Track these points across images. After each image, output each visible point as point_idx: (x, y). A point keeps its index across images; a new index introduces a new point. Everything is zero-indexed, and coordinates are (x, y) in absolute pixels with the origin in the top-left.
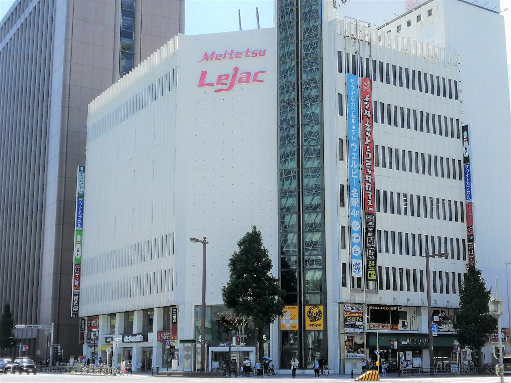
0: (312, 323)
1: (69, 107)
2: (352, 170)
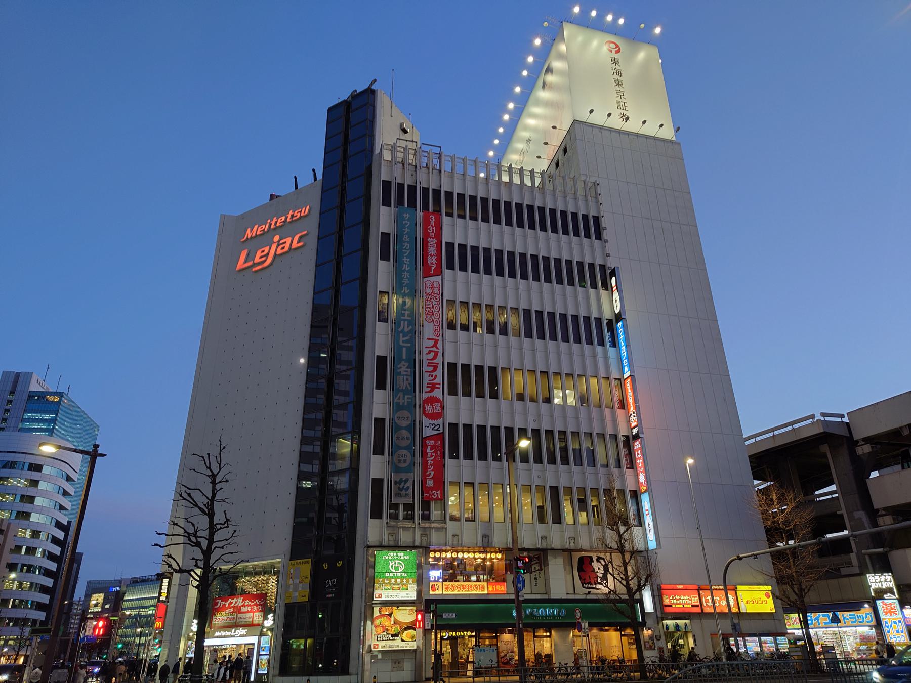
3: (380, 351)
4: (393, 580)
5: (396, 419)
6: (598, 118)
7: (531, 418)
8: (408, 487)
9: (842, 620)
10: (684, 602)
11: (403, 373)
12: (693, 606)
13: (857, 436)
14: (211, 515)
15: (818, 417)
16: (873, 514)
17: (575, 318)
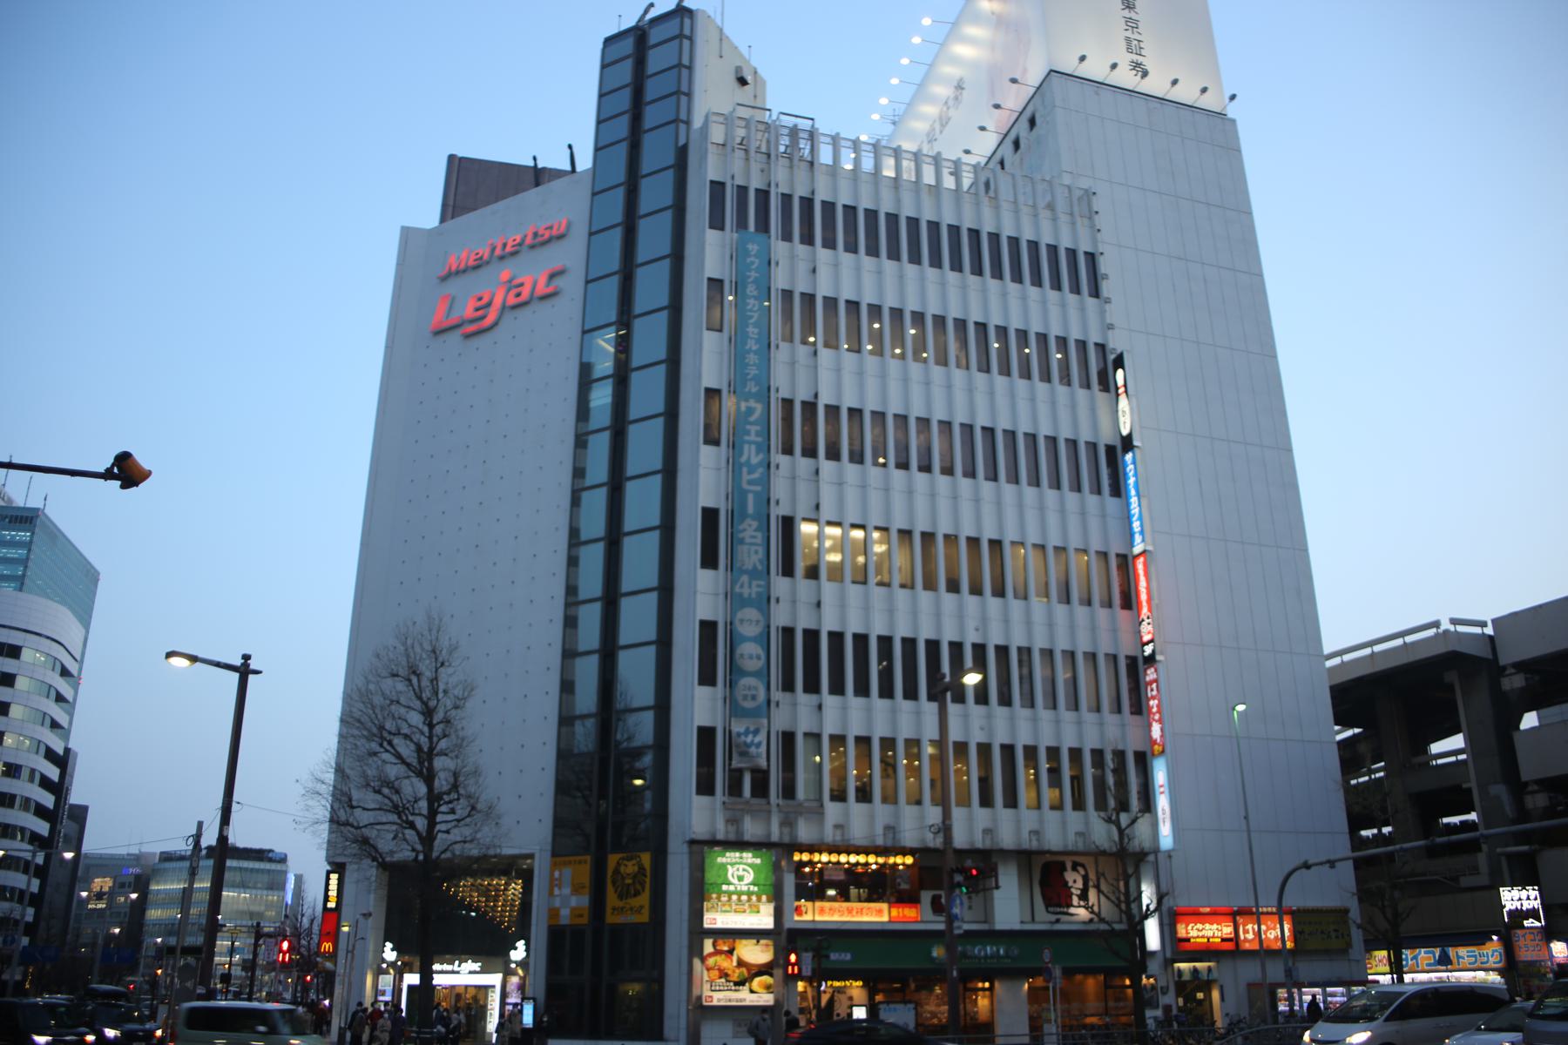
1: (1249, 831)
3: (707, 499)
4: (734, 897)
5: (737, 622)
6: (1095, 69)
7: (971, 624)
9: (1455, 960)
10: (1210, 934)
11: (748, 540)
12: (1223, 940)
13: (1504, 660)
14: (429, 778)
15: (1446, 625)
16: (1518, 788)
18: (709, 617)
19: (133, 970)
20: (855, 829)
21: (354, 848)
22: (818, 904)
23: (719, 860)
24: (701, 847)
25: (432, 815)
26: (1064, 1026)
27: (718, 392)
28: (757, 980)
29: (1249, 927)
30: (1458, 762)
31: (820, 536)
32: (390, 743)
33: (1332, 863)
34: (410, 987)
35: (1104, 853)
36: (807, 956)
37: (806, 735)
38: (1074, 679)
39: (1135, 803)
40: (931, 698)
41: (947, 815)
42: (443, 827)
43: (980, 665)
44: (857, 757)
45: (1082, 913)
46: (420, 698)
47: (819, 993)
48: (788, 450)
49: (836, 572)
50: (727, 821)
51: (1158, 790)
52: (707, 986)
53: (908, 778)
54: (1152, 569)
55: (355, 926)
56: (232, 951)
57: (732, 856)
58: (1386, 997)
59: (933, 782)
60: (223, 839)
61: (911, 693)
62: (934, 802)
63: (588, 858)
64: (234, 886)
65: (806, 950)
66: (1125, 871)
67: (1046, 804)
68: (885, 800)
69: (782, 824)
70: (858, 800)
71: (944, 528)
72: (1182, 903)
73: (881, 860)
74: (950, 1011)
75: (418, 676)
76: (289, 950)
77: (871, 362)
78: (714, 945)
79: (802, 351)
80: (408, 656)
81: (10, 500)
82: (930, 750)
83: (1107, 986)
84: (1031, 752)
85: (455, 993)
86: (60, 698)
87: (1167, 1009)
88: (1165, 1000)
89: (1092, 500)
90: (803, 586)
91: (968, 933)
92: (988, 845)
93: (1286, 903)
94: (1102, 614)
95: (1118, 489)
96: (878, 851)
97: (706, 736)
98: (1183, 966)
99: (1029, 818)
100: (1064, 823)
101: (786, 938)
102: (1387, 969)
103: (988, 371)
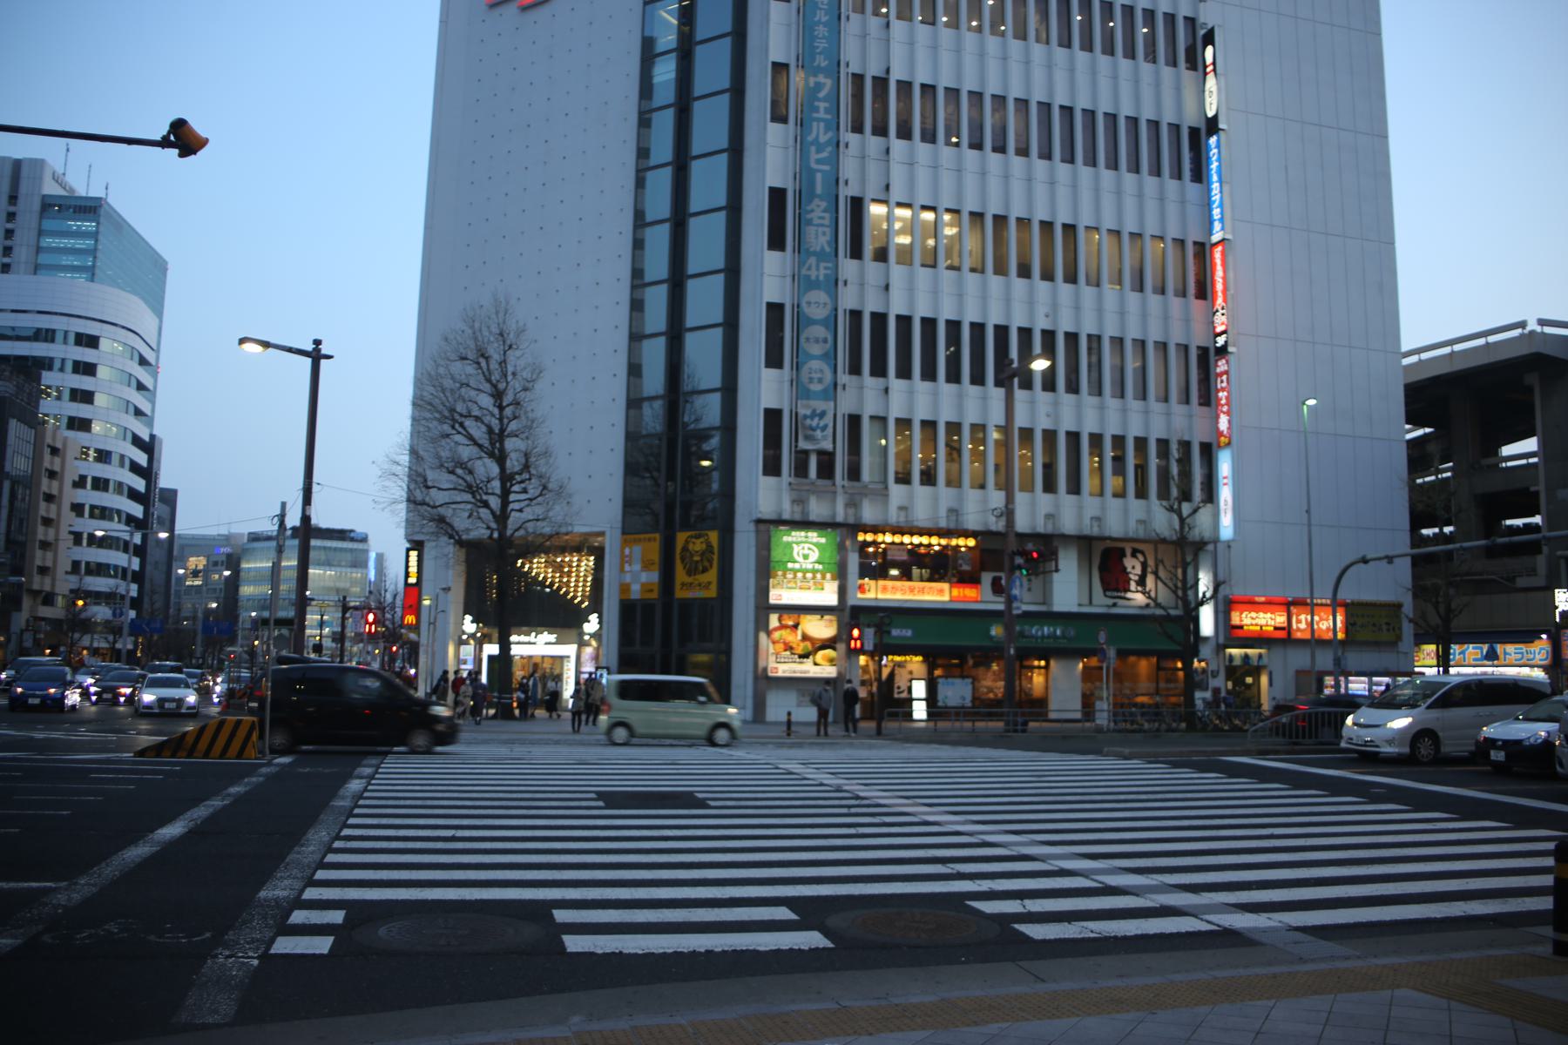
0: (690, 580)
1: (1309, 525)
2: (813, 149)
3: (774, 179)
4: (800, 575)
5: (804, 305)
7: (1041, 310)
8: (825, 427)
10: (1263, 622)
11: (816, 221)
12: (1276, 628)
14: (501, 459)
15: (1533, 326)
17: (1133, 121)
18: (776, 299)
19: (232, 641)
20: (918, 510)
21: (432, 527)
22: (881, 583)
23: (785, 539)
24: (767, 526)
25: (505, 494)
26: (1115, 705)
27: (786, 66)
28: (821, 653)
29: (1303, 617)
30: (1529, 464)
31: (889, 218)
32: (461, 425)
33: (1390, 559)
34: (491, 658)
35: (1164, 541)
36: (870, 632)
37: (872, 417)
38: (1144, 368)
39: (1197, 493)
40: (998, 383)
41: (1010, 499)
42: (516, 506)
43: (1049, 351)
44: (923, 441)
45: (1138, 598)
46: (489, 381)
47: (880, 666)
48: (858, 128)
49: (906, 255)
50: (793, 502)
51: (1222, 481)
52: (772, 658)
53: (972, 462)
54: (1230, 259)
55: (436, 599)
56: (322, 624)
57: (797, 535)
58: (1430, 686)
59: (997, 467)
60: (306, 519)
61: (978, 379)
62: (998, 487)
63: (657, 536)
64: (320, 564)
65: (869, 626)
66: (1184, 560)
67: (1109, 491)
68: (949, 484)
69: (847, 505)
70: (922, 483)
71: (1017, 211)
72: (1238, 591)
73: (944, 542)
74: (1006, 687)
75: (487, 359)
76: (374, 622)
77: (946, 35)
78: (780, 620)
79: (874, 23)
80: (476, 339)
81: (72, 190)
82: (996, 435)
83: (1159, 668)
84: (1096, 440)
85: (534, 665)
86: (141, 387)
87: (1216, 691)
88: (1214, 683)
89: (1171, 185)
90: (872, 268)
91: (1027, 614)
92: (1050, 530)
93: (1341, 596)
94: (1176, 303)
95: (1199, 174)
96: (941, 533)
97: (773, 418)
98: (1235, 651)
99: (1091, 505)
100: (1126, 511)
101: (850, 615)
102: (1434, 662)
103: (1069, 46)
